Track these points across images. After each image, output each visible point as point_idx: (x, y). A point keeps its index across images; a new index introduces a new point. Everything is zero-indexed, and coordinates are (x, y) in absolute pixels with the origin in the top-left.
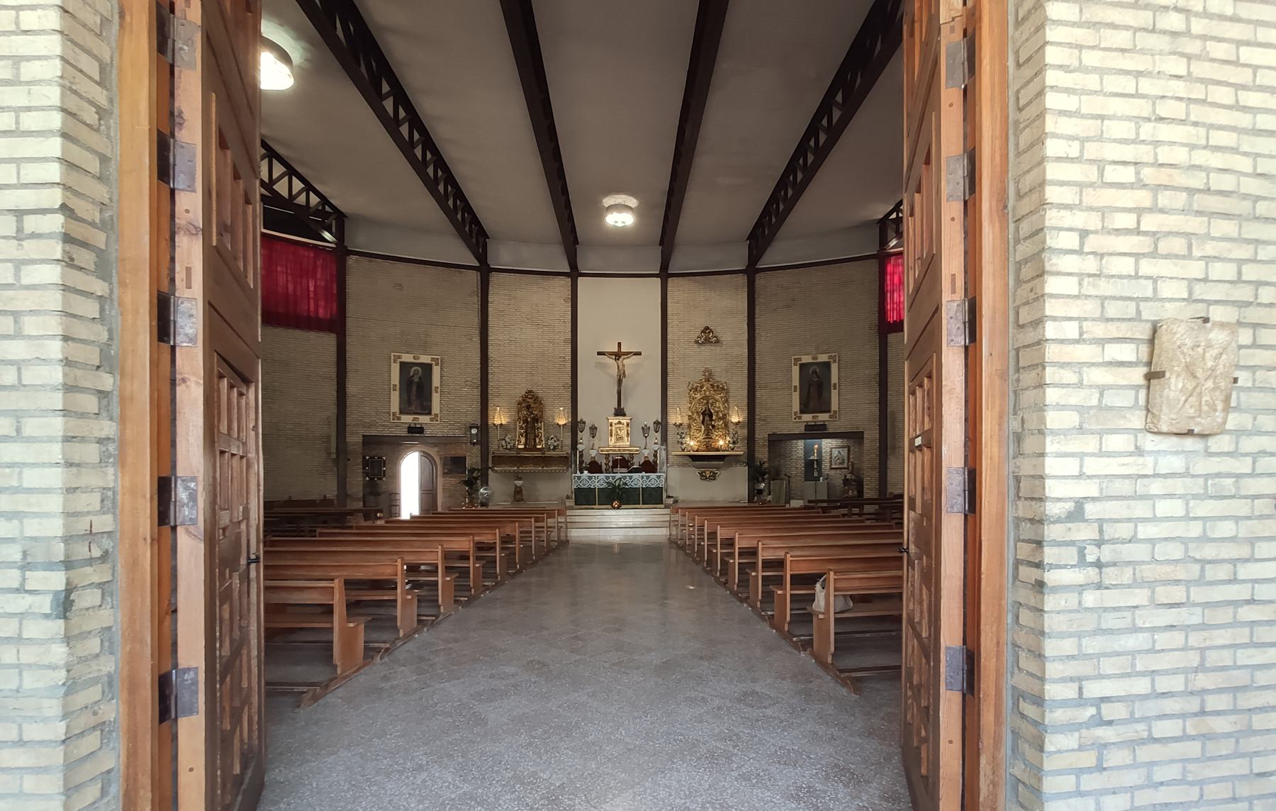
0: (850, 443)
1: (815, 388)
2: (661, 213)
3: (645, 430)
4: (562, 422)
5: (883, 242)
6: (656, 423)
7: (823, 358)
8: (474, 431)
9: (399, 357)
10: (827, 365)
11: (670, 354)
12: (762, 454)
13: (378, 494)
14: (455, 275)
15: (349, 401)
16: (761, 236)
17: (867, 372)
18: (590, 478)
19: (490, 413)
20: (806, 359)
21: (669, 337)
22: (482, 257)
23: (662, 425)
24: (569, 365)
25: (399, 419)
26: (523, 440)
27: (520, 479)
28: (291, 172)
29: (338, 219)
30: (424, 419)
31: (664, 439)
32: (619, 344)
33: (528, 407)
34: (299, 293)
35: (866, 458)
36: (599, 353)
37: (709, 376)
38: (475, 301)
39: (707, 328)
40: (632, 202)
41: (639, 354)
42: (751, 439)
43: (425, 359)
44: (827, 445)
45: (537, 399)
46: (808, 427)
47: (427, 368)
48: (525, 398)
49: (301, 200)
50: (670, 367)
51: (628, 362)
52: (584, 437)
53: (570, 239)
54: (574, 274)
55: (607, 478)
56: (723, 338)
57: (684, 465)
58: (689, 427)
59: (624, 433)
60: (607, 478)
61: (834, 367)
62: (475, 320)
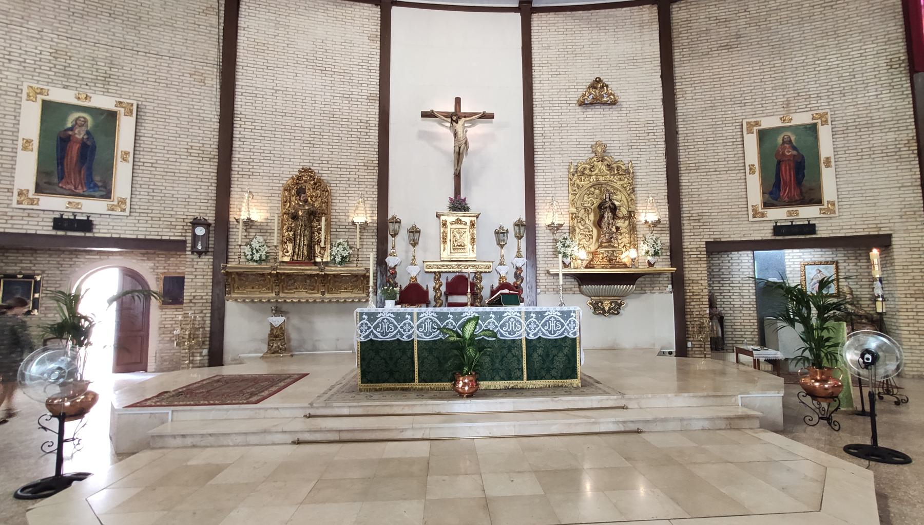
3: (500, 235)
4: (360, 219)
6: (518, 224)
7: (802, 119)
8: (200, 231)
10: (812, 130)
11: (537, 122)
17: (891, 136)
20: (769, 123)
23: (528, 227)
26: (290, 247)
32: (458, 101)
35: (900, 278)
36: (425, 115)
37: (601, 153)
42: (676, 252)
43: (104, 102)
45: (318, 184)
46: (778, 230)
47: (107, 120)
51: (475, 132)
52: (399, 246)
55: (442, 317)
58: (572, 230)
59: (467, 239)
60: (442, 317)
61: (824, 133)
62: (213, 53)
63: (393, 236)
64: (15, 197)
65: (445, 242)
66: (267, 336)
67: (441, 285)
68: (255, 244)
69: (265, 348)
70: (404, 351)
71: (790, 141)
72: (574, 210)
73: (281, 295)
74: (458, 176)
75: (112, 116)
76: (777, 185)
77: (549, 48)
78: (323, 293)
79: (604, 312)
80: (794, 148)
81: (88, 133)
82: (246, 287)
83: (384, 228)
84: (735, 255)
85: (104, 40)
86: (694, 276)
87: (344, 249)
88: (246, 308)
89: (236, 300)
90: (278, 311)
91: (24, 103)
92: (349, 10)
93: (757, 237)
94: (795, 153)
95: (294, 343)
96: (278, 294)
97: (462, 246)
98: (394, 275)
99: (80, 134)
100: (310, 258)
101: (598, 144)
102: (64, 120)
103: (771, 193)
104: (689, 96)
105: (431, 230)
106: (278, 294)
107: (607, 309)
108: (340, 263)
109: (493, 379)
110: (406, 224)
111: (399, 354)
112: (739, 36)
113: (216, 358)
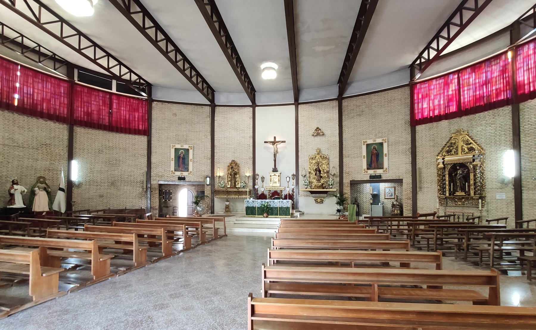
0: (396, 185)
1: (375, 156)
2: (289, 71)
5: (412, 76)
6: (293, 175)
7: (379, 141)
10: (381, 144)
12: (347, 190)
16: (344, 80)
18: (253, 202)
20: (370, 142)
21: (299, 133)
22: (212, 101)
25: (174, 173)
26: (230, 183)
27: (228, 201)
28: (120, 64)
29: (149, 87)
30: (185, 174)
31: (297, 183)
32: (275, 138)
33: (232, 168)
34: (131, 119)
35: (404, 193)
36: (265, 142)
38: (209, 120)
39: (318, 128)
40: (275, 66)
43: (186, 147)
44: (382, 186)
45: (236, 164)
46: (371, 177)
49: (127, 77)
51: (280, 146)
52: (259, 181)
53: (251, 90)
54: (254, 105)
55: (262, 202)
56: (326, 133)
57: (307, 196)
59: (277, 180)
60: (262, 202)
61: (385, 146)
62: (209, 129)
69: (224, 211)
74: (275, 161)
75: (188, 150)
80: (376, 150)
83: (254, 177)
85: (185, 130)
86: (346, 192)
88: (219, 200)
90: (227, 201)
95: (231, 210)
97: (276, 182)
98: (257, 191)
99: (182, 156)
101: (318, 149)
104: (347, 132)
110: (260, 176)
113: (213, 212)
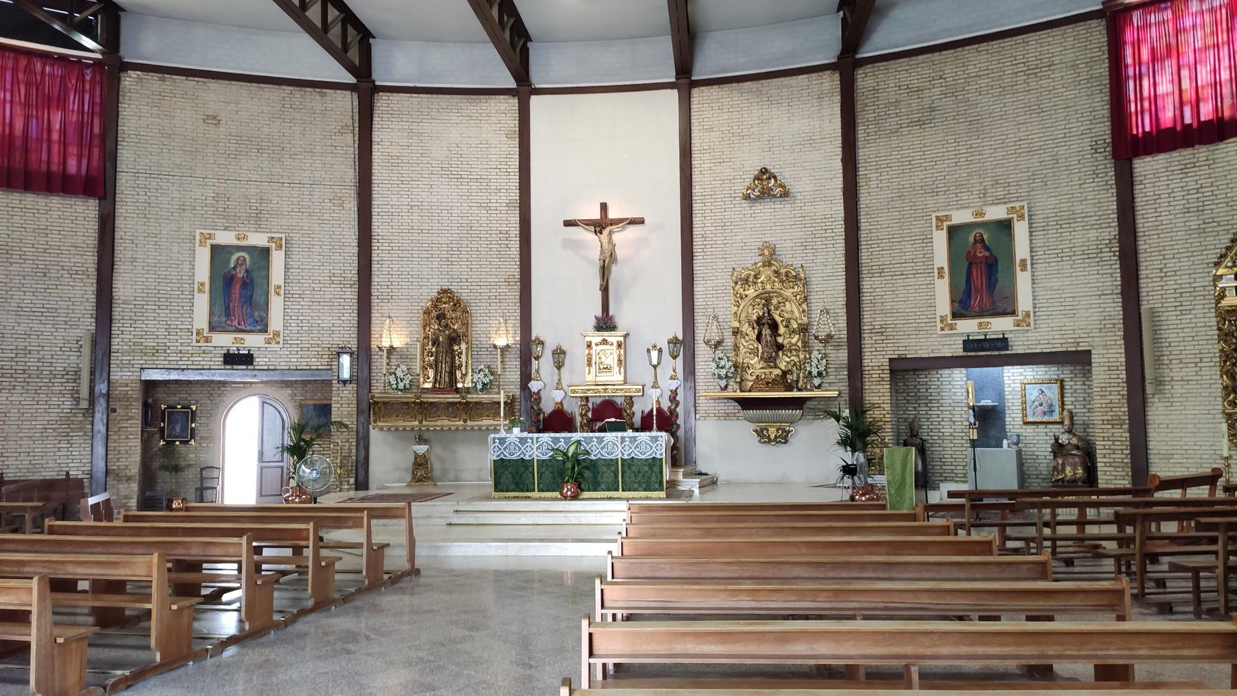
0: (1065, 373)
1: (981, 269)
4: (501, 341)
6: (674, 342)
7: (996, 213)
9: (210, 237)
10: (1005, 226)
12: (878, 394)
13: (176, 469)
14: (312, 98)
15: (117, 312)
18: (523, 441)
19: (375, 328)
20: (961, 217)
21: (696, 190)
24: (515, 245)
26: (431, 373)
30: (252, 341)
31: (690, 370)
32: (604, 207)
33: (441, 317)
35: (1097, 402)
36: (568, 223)
37: (770, 257)
38: (349, 141)
39: (764, 171)
41: (640, 221)
43: (258, 239)
44: (1013, 377)
45: (457, 304)
46: (969, 344)
48: (436, 302)
50: (698, 242)
51: (623, 237)
52: (544, 366)
54: (524, 88)
55: (556, 440)
56: (795, 187)
57: (727, 416)
60: (556, 440)
61: (1021, 231)
62: (349, 174)
63: (537, 358)
64: (194, 337)
65: (589, 365)
66: (411, 465)
67: (677, 405)
68: (399, 373)
69: (409, 477)
70: (526, 468)
71: (982, 240)
72: (736, 324)
73: (424, 423)
74: (605, 290)
75: (265, 252)
76: (968, 292)
77: (711, 130)
78: (465, 421)
79: (770, 441)
80: (987, 248)
81: (247, 271)
82: (391, 415)
83: (527, 350)
84: (946, 372)
86: (875, 400)
87: (486, 375)
88: (389, 436)
89: (382, 429)
90: (421, 440)
91: (198, 249)
92: (484, 106)
93: (947, 352)
94: (987, 254)
95: (437, 473)
96: (421, 422)
98: (539, 400)
99: (241, 273)
100: (452, 386)
101: (767, 246)
102: (229, 260)
103: (960, 302)
104: (873, 184)
105: (576, 353)
106: (421, 422)
107: (772, 437)
108: (482, 390)
109: (595, 490)
110: (550, 345)
111: (522, 469)
112: (932, 109)
